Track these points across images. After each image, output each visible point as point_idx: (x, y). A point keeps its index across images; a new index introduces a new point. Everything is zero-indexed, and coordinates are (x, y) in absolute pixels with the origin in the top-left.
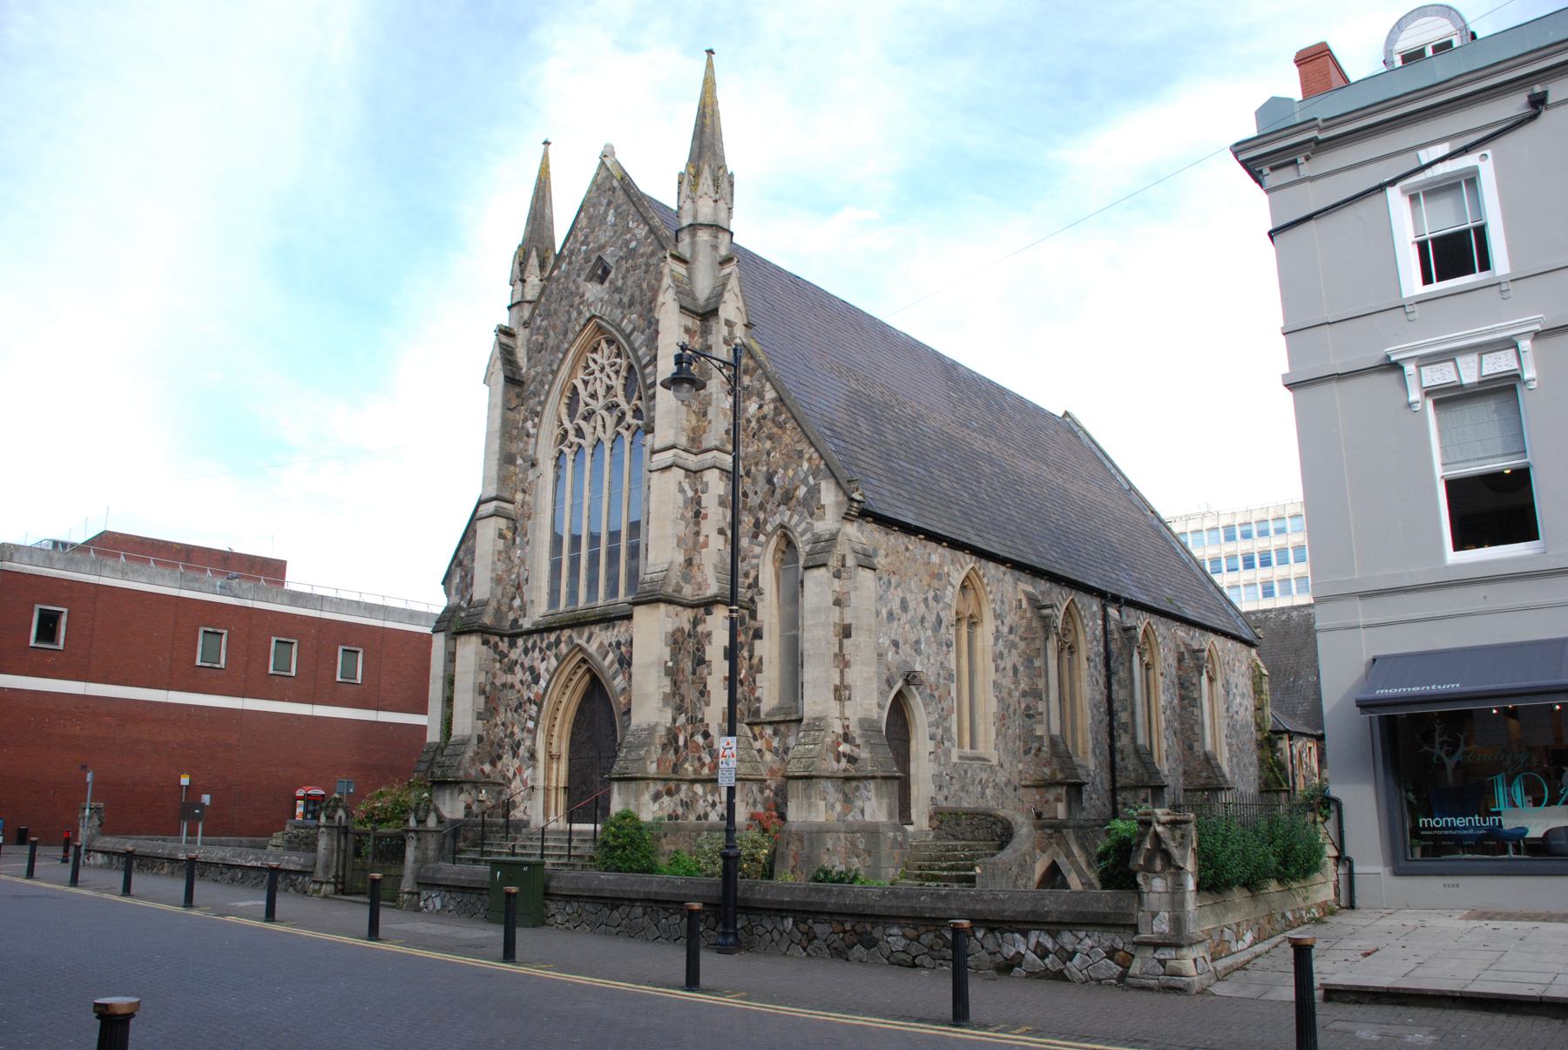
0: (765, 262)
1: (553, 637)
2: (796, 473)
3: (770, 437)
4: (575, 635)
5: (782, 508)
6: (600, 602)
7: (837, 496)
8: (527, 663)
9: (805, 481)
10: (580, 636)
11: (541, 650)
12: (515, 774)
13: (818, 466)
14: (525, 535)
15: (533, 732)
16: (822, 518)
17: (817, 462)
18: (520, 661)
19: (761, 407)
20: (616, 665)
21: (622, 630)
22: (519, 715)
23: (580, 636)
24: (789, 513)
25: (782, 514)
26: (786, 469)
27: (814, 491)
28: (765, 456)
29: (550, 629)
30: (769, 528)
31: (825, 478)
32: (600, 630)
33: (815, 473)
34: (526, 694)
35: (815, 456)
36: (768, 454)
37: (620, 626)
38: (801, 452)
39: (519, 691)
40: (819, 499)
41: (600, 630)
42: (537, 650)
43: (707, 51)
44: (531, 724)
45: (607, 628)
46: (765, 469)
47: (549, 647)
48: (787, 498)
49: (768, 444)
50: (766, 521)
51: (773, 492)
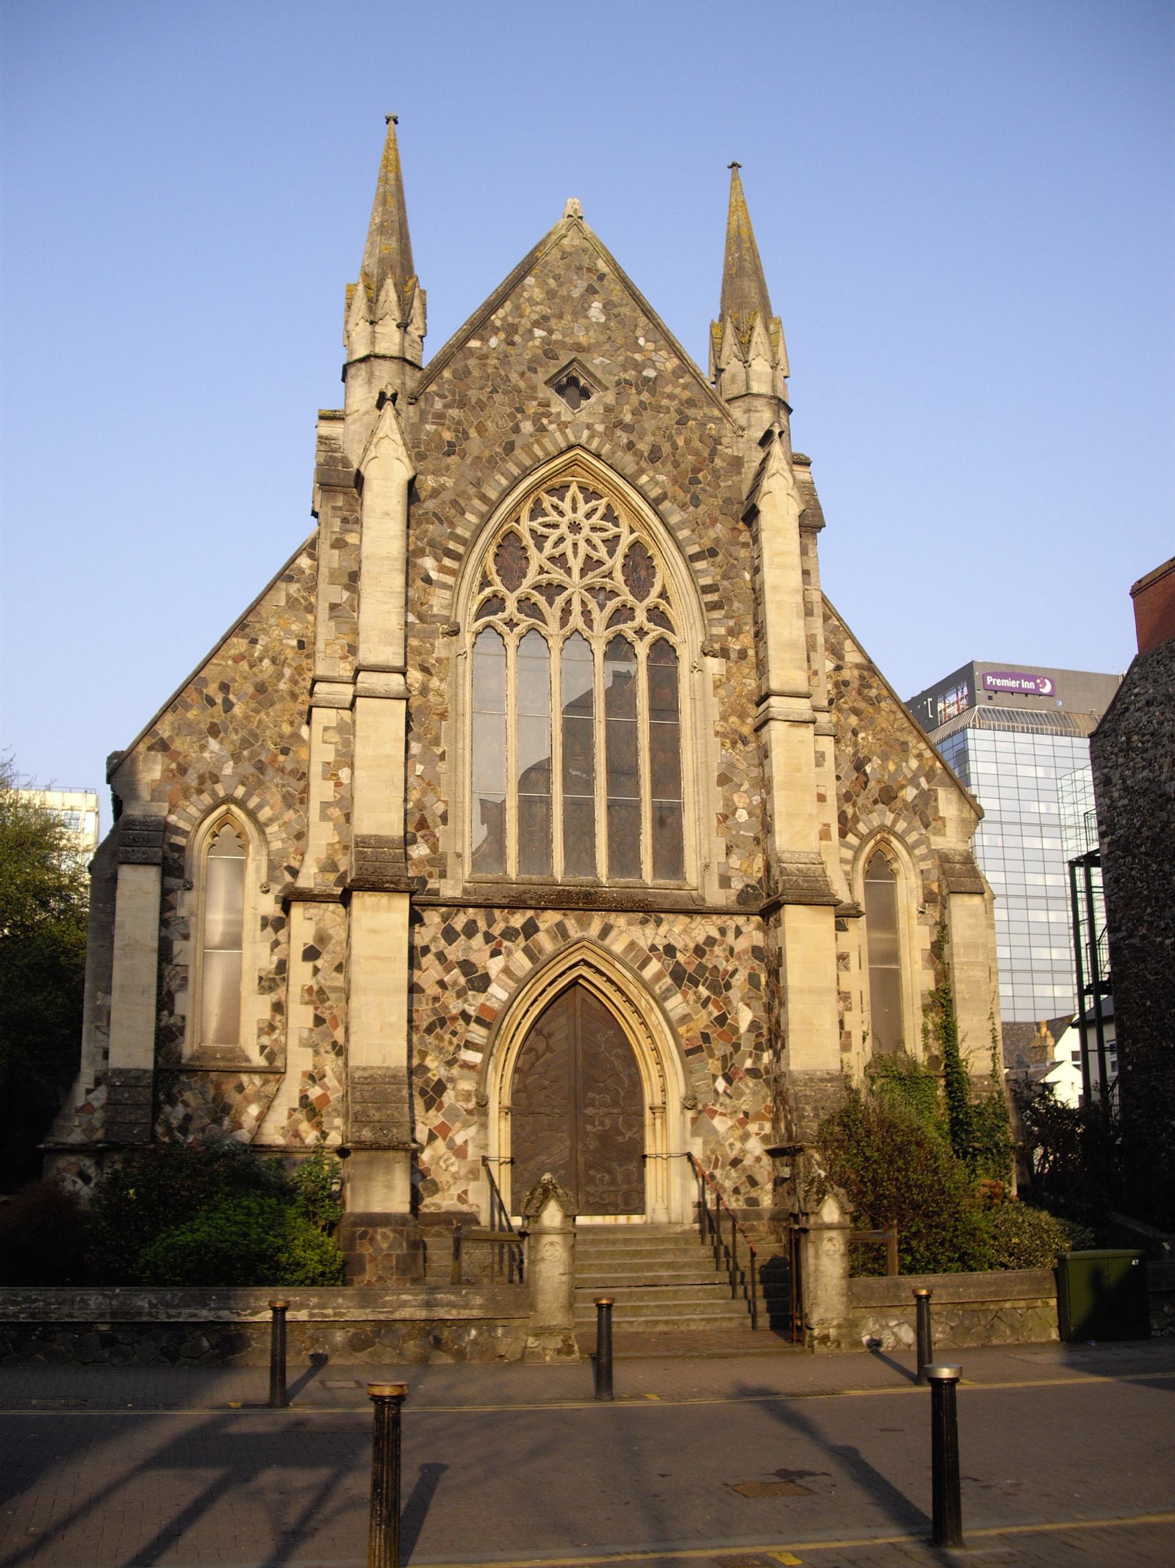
0: (1137, 621)
1: (518, 920)
2: (899, 768)
3: (856, 712)
4: (571, 924)
5: (880, 806)
6: (512, 869)
7: (961, 811)
8: (454, 952)
9: (913, 781)
10: (583, 925)
11: (488, 938)
12: (432, 1137)
13: (932, 769)
14: (436, 741)
15: (480, 1072)
16: (940, 832)
17: (930, 763)
18: (433, 949)
19: (838, 668)
20: (668, 981)
21: (677, 930)
22: (440, 1038)
23: (583, 925)
24: (892, 816)
25: (883, 814)
26: (885, 758)
27: (927, 798)
28: (850, 735)
29: (515, 905)
30: (862, 828)
31: (943, 785)
32: (629, 924)
33: (930, 775)
34: (455, 1006)
35: (928, 754)
36: (855, 733)
37: (672, 924)
38: (905, 743)
39: (436, 999)
40: (936, 808)
41: (629, 924)
42: (479, 937)
43: (730, 167)
44: (475, 1057)
45: (644, 922)
46: (850, 750)
47: (509, 934)
48: (888, 796)
49: (853, 720)
50: (856, 819)
51: (866, 783)
